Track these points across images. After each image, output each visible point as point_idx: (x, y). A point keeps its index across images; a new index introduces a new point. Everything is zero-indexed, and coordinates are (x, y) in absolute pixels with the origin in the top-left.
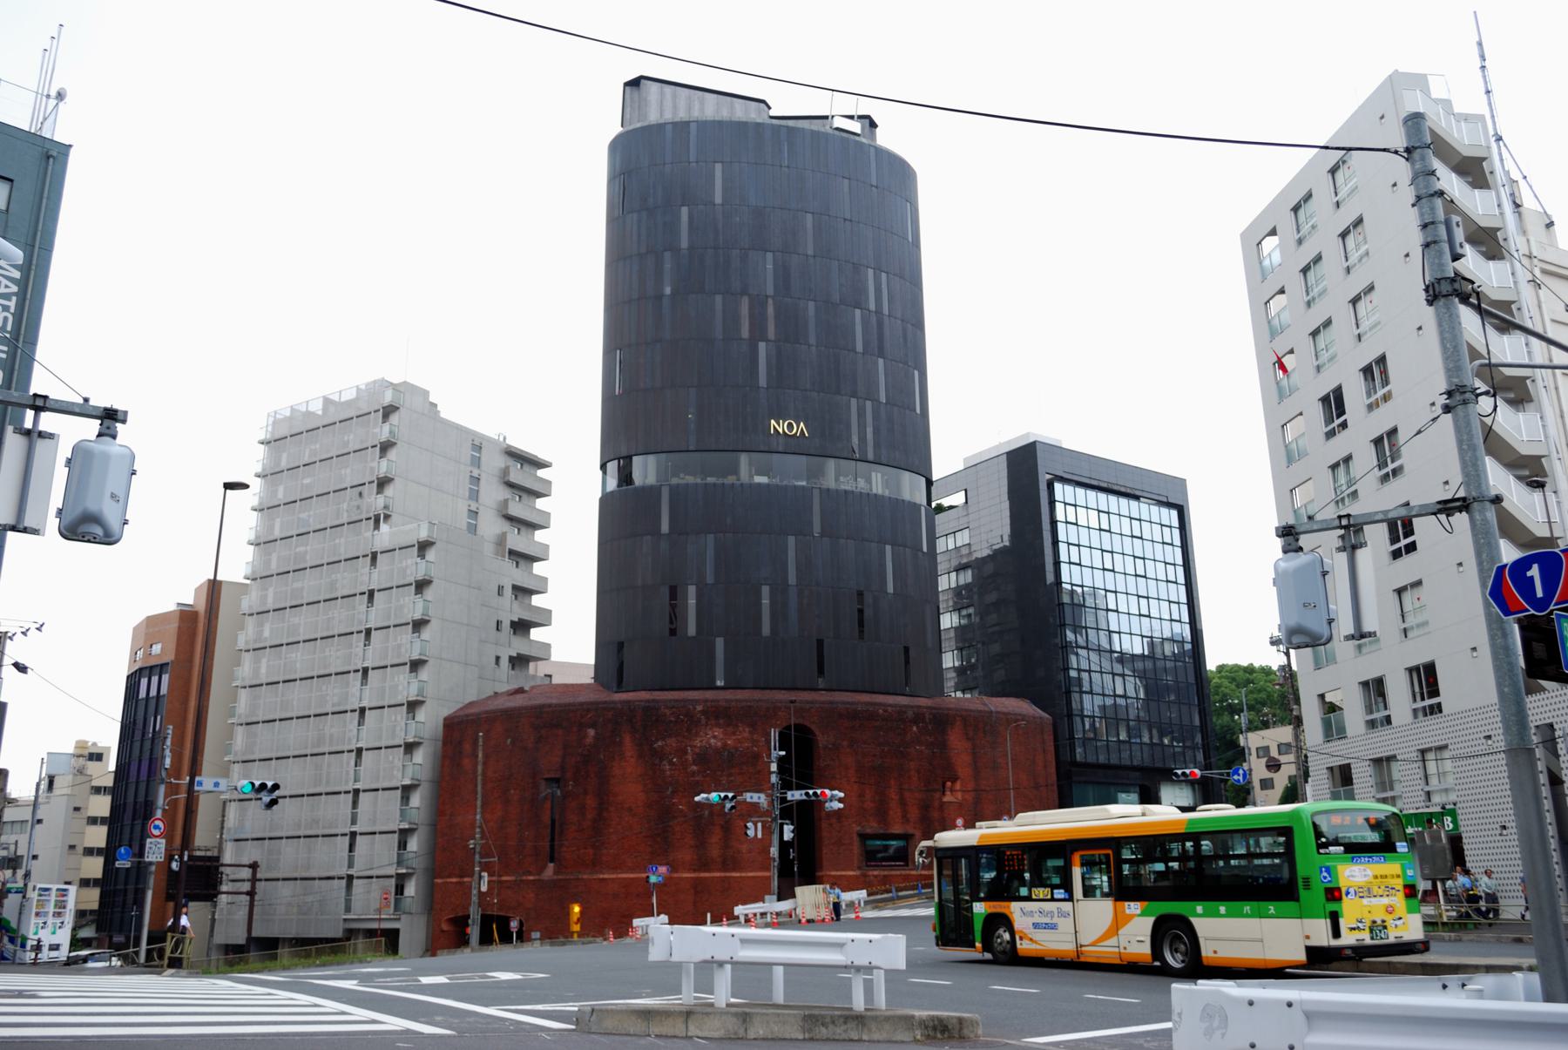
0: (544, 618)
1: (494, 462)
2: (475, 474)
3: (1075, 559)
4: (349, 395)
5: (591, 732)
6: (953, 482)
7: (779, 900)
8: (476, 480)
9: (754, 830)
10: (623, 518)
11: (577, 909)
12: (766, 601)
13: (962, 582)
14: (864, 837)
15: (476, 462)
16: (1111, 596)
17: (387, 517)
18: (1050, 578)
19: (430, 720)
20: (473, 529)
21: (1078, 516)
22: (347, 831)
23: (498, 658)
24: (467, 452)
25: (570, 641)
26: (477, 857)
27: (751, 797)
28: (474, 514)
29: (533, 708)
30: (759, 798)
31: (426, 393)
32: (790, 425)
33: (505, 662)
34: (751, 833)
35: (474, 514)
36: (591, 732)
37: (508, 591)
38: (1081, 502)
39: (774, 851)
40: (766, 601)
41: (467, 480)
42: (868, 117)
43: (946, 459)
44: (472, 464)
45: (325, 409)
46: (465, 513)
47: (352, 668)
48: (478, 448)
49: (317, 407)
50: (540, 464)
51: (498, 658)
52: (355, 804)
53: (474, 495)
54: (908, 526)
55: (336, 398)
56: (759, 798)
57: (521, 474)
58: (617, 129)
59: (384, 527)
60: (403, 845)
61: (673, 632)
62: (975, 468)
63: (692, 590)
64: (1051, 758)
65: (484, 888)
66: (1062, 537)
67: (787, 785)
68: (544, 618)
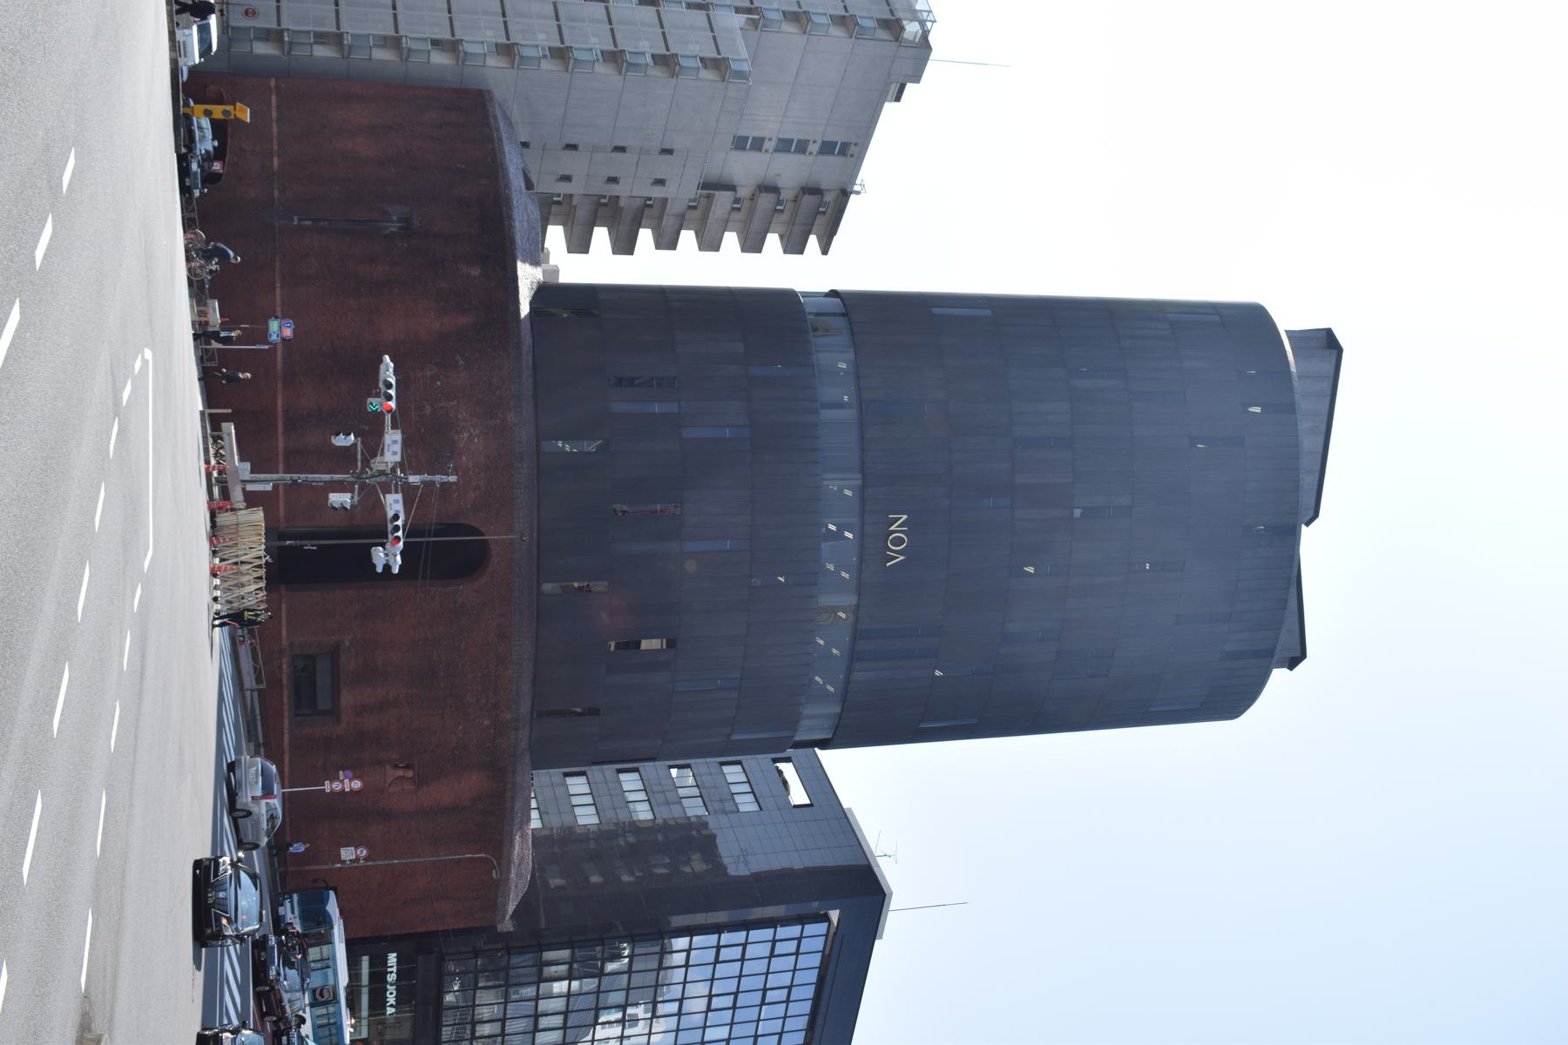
3: (725, 954)
6: (817, 781)
10: (777, 308)
11: (347, 854)
13: (738, 799)
14: (334, 653)
16: (674, 1007)
17: (755, 23)
18: (677, 921)
19: (495, 74)
20: (740, 143)
21: (788, 955)
27: (393, 441)
29: (508, 202)
30: (393, 445)
31: (917, 78)
32: (901, 541)
42: (1303, 656)
43: (848, 769)
48: (844, 150)
50: (898, 99)
53: (784, 146)
56: (393, 445)
57: (815, 213)
59: (740, 20)
60: (321, 38)
61: (619, 382)
62: (827, 809)
63: (672, 408)
64: (451, 924)
66: (755, 935)
67: (409, 493)
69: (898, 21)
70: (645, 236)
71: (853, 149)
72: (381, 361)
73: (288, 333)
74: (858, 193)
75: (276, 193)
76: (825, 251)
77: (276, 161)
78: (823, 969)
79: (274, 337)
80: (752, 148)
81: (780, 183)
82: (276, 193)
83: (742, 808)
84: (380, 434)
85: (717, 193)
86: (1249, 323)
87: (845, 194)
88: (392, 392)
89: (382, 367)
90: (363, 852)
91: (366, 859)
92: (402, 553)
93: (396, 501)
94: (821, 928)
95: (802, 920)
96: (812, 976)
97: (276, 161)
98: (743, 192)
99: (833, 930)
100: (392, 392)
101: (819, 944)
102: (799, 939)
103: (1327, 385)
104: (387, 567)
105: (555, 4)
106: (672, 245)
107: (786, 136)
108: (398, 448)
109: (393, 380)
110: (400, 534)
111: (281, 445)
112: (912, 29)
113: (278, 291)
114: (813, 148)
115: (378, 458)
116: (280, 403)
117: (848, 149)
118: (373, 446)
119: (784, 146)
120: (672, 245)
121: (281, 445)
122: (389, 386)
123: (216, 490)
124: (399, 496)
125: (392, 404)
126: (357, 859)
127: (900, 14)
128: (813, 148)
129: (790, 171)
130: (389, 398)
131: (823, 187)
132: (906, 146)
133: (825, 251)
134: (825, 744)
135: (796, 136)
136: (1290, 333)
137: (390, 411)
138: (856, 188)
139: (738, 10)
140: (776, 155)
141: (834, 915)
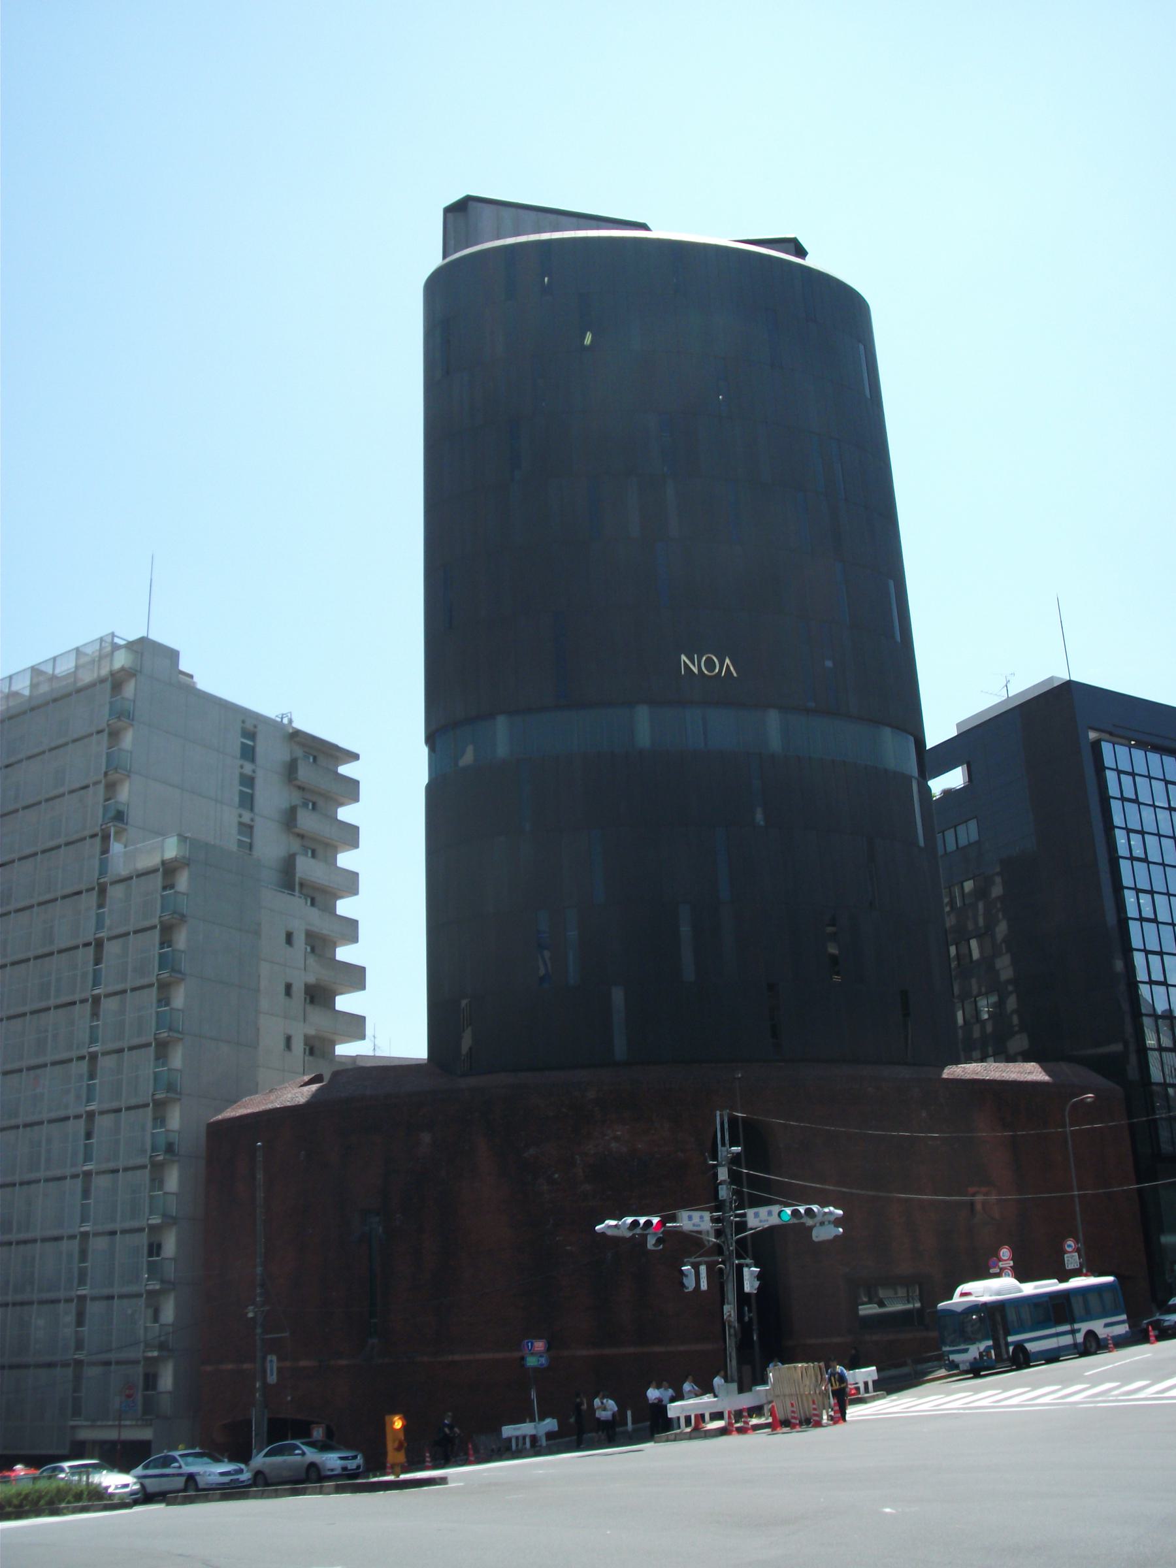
0: (355, 977)
1: (271, 754)
2: (246, 817)
4: (65, 667)
5: (426, 1137)
7: (741, 1390)
8: (248, 781)
9: (695, 1276)
12: (685, 929)
13: (963, 842)
15: (248, 753)
22: (87, 994)
23: (288, 1040)
24: (235, 742)
25: (392, 1019)
26: (259, 1331)
28: (247, 829)
30: (695, 1220)
33: (298, 1046)
34: (690, 1283)
35: (247, 829)
36: (426, 1137)
37: (300, 940)
38: (1140, 768)
39: (729, 1310)
40: (685, 929)
41: (236, 781)
44: (242, 804)
45: (33, 686)
46: (234, 830)
47: (80, 941)
48: (252, 736)
49: (23, 686)
51: (288, 1040)
52: (95, 1014)
53: (247, 801)
54: (888, 793)
55: (48, 669)
56: (695, 1220)
57: (313, 772)
58: (433, 259)
62: (975, 742)
65: (272, 1379)
68: (355, 977)
69: (112, 674)
70: (344, 954)
71: (249, 726)
72: (603, 1233)
73: (540, 1345)
74: (291, 721)
75: (344, 1362)
76: (355, 757)
77: (303, 1363)
78: (1142, 745)
79: (543, 1360)
80: (251, 836)
81: (285, 805)
82: (344, 1362)
83: (974, 836)
84: (679, 1234)
85: (298, 875)
86: (440, 289)
87: (298, 738)
88: (642, 1220)
89: (609, 1232)
90: (1070, 1244)
91: (1077, 1242)
92: (823, 1206)
93: (756, 1215)
94: (1106, 748)
95: (1100, 768)
96: (1154, 757)
97: (303, 1363)
98: (295, 845)
99: (1107, 736)
100: (642, 1220)
101: (1122, 751)
102: (1119, 772)
103: (506, 213)
104: (838, 1222)
105: (5, 1073)
106: (352, 925)
107: (237, 799)
108: (696, 1215)
109: (629, 1220)
110: (802, 1209)
111: (631, 1350)
112: (121, 660)
113: (457, 1357)
114: (248, 768)
115: (704, 1237)
116: (584, 1352)
117: (250, 731)
118: (689, 1244)
119: (247, 801)
120: (352, 925)
121: (631, 1350)
122: (635, 1224)
123: (754, 1421)
124: (750, 1212)
125: (655, 1220)
126: (1078, 1250)
127: (104, 672)
128: (248, 768)
129: (272, 796)
130: (648, 1224)
131: (288, 758)
132: (237, 668)
133: (355, 757)
134: (920, 741)
135: (237, 788)
136: (444, 257)
137: (662, 1223)
138: (285, 721)
139: (105, 851)
140: (256, 810)
141: (1092, 735)
